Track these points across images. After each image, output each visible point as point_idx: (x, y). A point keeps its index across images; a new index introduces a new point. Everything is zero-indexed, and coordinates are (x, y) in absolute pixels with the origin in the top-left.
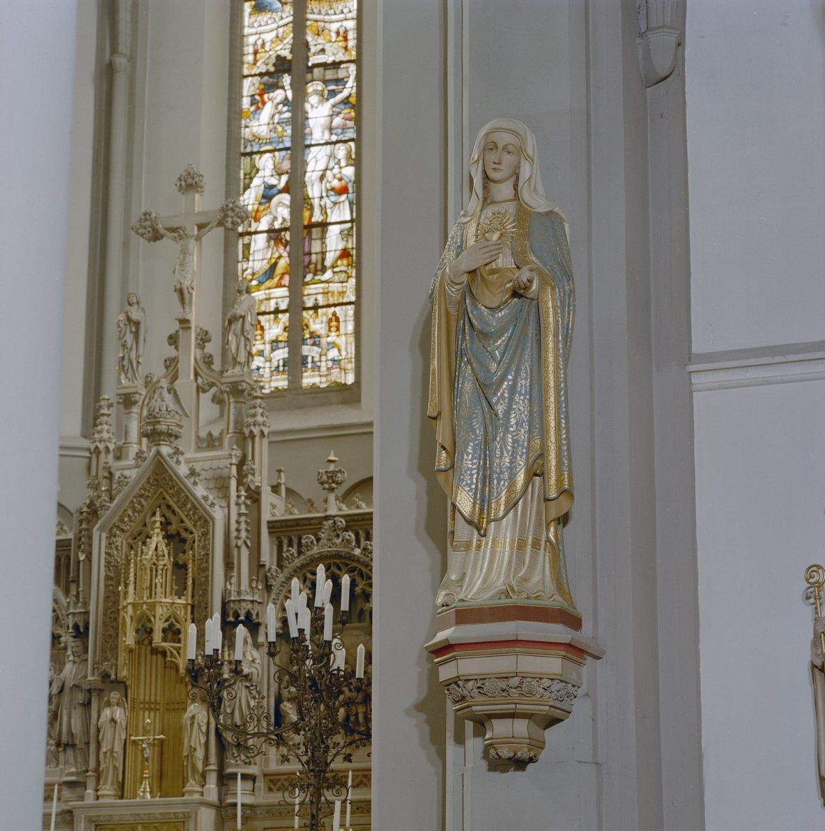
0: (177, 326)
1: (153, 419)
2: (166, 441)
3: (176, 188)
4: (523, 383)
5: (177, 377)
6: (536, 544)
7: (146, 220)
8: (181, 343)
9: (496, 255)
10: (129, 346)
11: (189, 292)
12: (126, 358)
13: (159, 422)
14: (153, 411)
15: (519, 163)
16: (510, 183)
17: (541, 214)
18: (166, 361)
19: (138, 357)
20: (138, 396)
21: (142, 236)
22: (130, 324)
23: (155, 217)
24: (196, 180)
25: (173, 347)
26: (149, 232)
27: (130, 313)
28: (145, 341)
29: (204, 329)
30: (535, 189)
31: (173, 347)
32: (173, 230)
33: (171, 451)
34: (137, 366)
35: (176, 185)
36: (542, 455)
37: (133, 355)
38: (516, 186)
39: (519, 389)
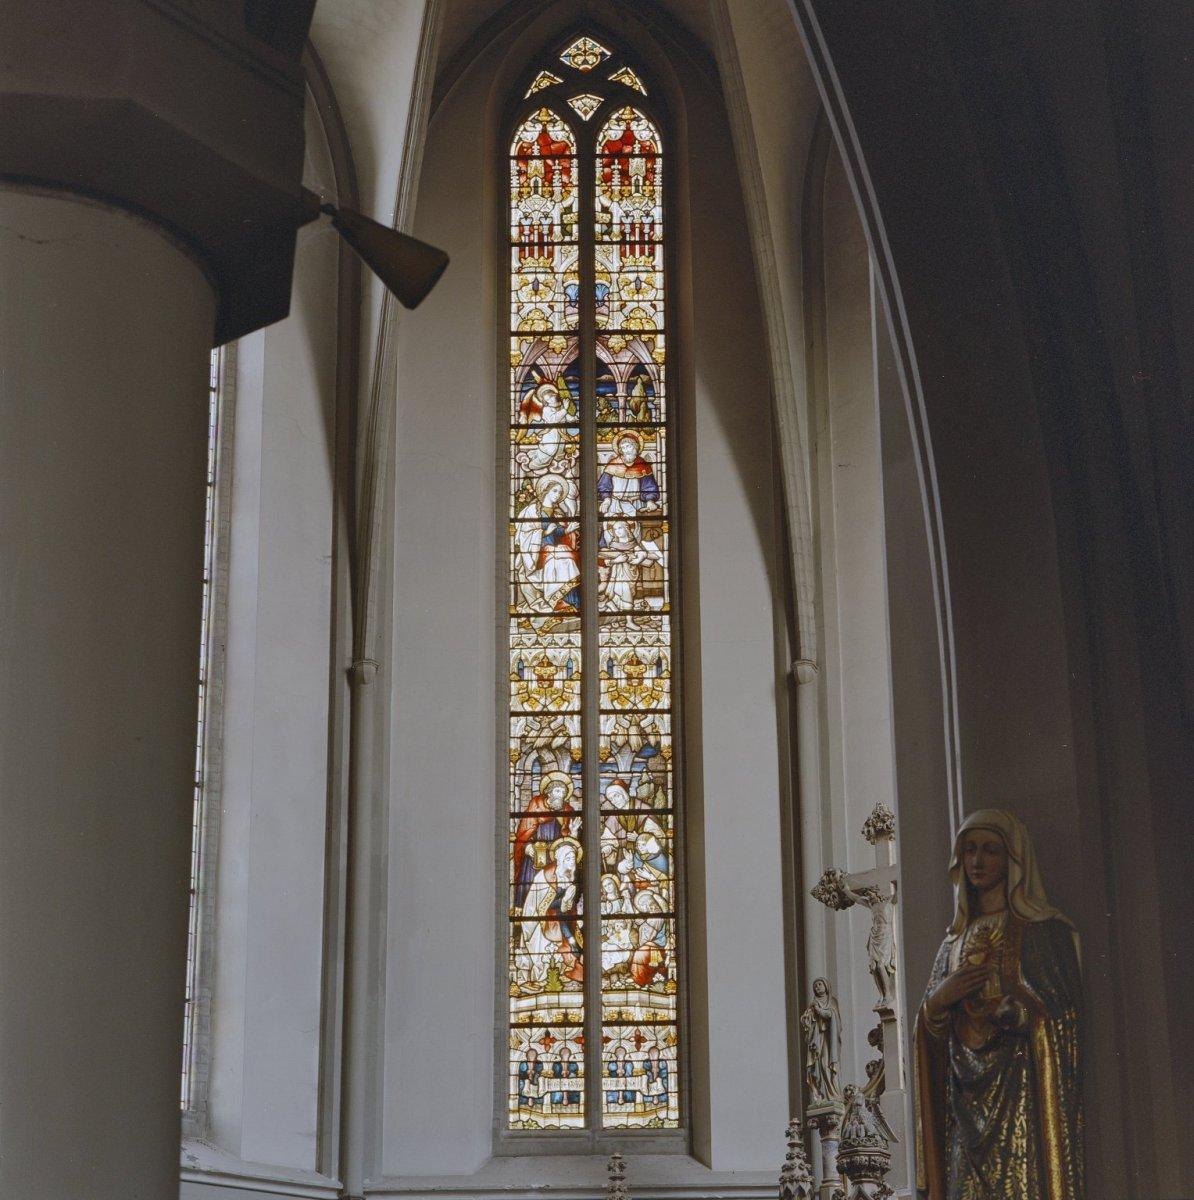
0: (877, 1019)
1: (848, 1148)
2: (869, 1177)
3: (864, 837)
5: (884, 1089)
7: (830, 882)
8: (886, 1040)
9: (980, 982)
10: (819, 1051)
11: (889, 973)
12: (817, 1069)
13: (857, 1151)
14: (849, 1138)
15: (1006, 868)
18: (868, 1067)
19: (831, 1064)
20: (834, 1116)
21: (826, 903)
22: (818, 1021)
23: (841, 877)
24: (888, 823)
25: (876, 1047)
26: (834, 897)
27: (817, 1007)
28: (840, 1041)
30: (1031, 891)
31: (876, 1047)
32: (862, 892)
33: (877, 1189)
34: (832, 1078)
35: (863, 833)
37: (825, 1063)
39: (1014, 1151)
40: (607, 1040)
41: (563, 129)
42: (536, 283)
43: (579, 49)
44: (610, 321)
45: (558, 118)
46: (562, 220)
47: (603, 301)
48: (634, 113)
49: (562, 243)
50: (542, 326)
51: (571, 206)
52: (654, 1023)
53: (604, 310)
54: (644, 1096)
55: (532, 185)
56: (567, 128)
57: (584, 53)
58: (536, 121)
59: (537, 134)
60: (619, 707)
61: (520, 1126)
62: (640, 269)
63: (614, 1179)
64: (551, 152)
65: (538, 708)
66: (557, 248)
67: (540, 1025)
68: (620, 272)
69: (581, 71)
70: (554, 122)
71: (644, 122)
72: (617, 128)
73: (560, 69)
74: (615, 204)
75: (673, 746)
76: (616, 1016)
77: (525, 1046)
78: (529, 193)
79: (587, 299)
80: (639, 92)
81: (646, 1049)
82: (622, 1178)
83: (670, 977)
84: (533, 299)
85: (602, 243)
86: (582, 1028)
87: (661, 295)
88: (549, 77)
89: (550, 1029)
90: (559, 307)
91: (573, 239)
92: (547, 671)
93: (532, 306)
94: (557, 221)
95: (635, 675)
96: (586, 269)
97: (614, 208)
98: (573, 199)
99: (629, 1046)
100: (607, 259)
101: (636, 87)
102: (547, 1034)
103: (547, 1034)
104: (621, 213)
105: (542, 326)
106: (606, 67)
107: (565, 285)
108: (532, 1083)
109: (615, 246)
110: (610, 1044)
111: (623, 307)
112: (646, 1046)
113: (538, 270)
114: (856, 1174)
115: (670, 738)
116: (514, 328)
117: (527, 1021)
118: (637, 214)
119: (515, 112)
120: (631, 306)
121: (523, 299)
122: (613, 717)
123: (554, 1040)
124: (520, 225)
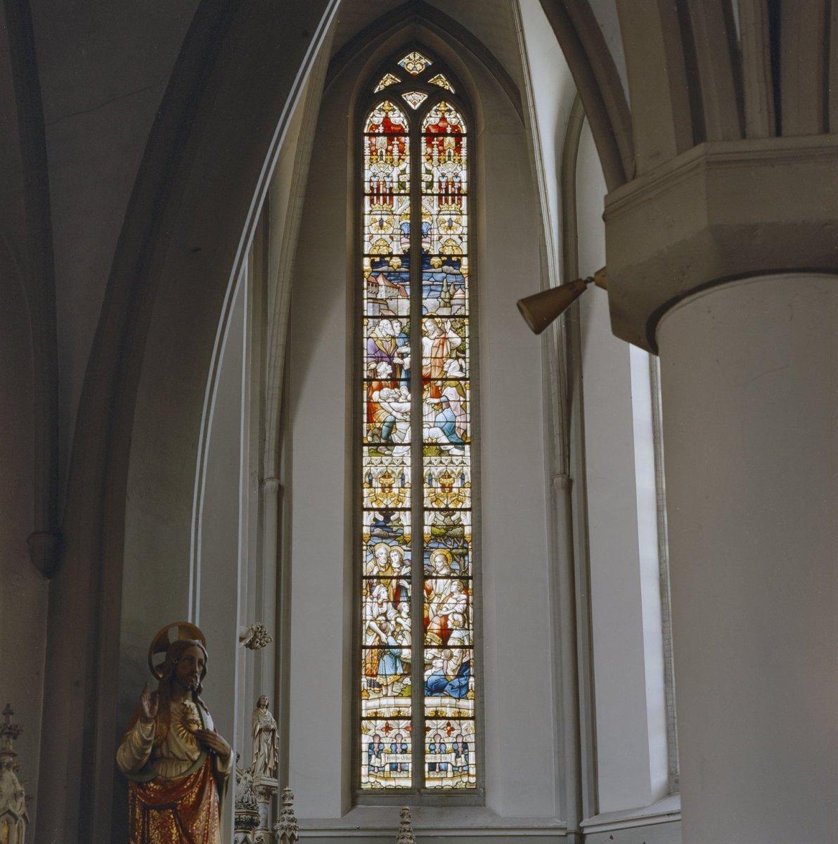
40: (429, 729)
41: (456, 117)
42: (450, 221)
43: (410, 59)
44: (400, 247)
45: (453, 109)
46: (399, 179)
47: (428, 234)
48: (447, 106)
49: (399, 194)
50: (386, 251)
51: (405, 170)
52: (460, 718)
53: (428, 240)
54: (453, 766)
55: (379, 154)
56: (402, 115)
57: (414, 63)
58: (380, 110)
59: (382, 119)
60: (435, 506)
61: (369, 786)
62: (452, 212)
63: (403, 823)
64: (391, 132)
65: (443, 506)
66: (395, 198)
67: (445, 718)
68: (438, 215)
69: (412, 75)
70: (394, 110)
71: (397, 112)
72: (379, 116)
73: (401, 72)
74: (435, 168)
75: (412, 534)
76: (434, 713)
77: (372, 733)
78: (377, 159)
79: (416, 231)
80: (449, 91)
81: (455, 735)
82: (408, 823)
83: (470, 688)
84: (380, 232)
85: (426, 194)
86: (410, 721)
87: (465, 231)
88: (392, 78)
89: (450, 721)
90: (396, 238)
91: (406, 192)
92: (387, 481)
93: (379, 237)
94: (395, 179)
95: (447, 485)
96: (416, 214)
97: (435, 171)
98: (406, 165)
99: (443, 733)
100: (429, 205)
101: (447, 87)
102: (449, 724)
103: (449, 724)
104: (439, 174)
105: (386, 251)
106: (429, 72)
107: (401, 223)
108: (377, 757)
109: (435, 197)
110: (431, 732)
111: (440, 238)
112: (455, 733)
113: (383, 212)
114: (248, 827)
115: (410, 528)
116: (366, 252)
117: (374, 715)
118: (381, 175)
119: (368, 102)
120: (445, 238)
121: (373, 232)
122: (433, 513)
123: (391, 729)
124: (440, 182)
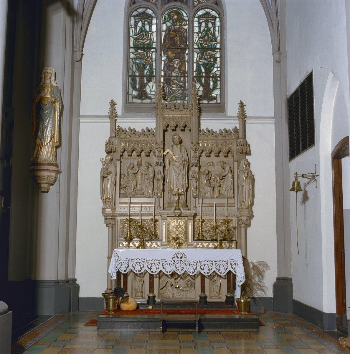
4: (51, 120)
6: (51, 151)
15: (51, 76)
16: (49, 80)
17: (55, 87)
29: (114, 101)
36: (54, 134)
38: (50, 80)
